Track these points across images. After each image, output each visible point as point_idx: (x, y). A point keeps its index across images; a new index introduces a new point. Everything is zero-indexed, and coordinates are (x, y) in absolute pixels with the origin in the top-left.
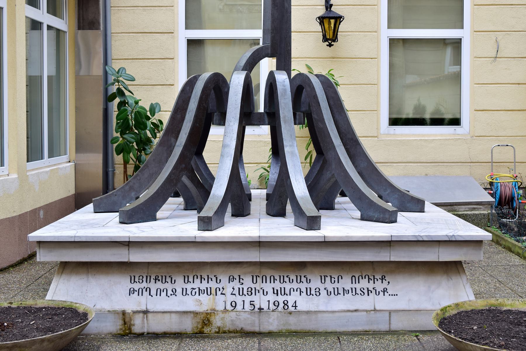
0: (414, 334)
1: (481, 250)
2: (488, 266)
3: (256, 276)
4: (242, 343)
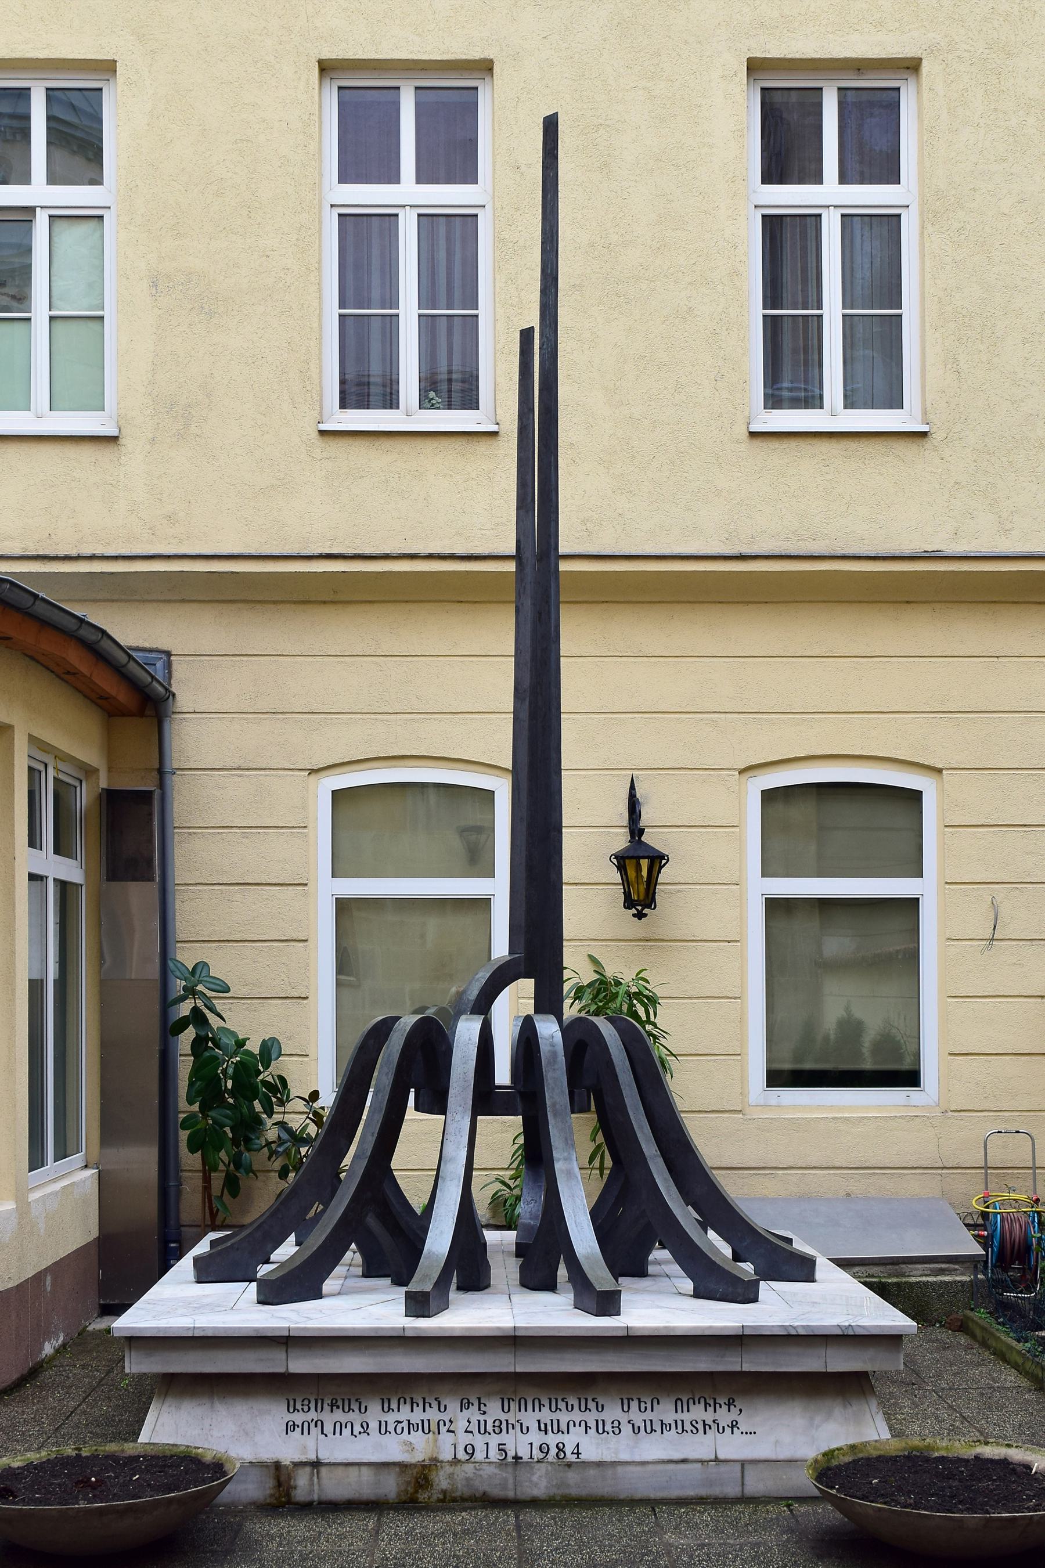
0: (784, 1503)
1: (899, 1352)
2: (950, 1389)
3: (509, 1400)
4: (486, 1516)
